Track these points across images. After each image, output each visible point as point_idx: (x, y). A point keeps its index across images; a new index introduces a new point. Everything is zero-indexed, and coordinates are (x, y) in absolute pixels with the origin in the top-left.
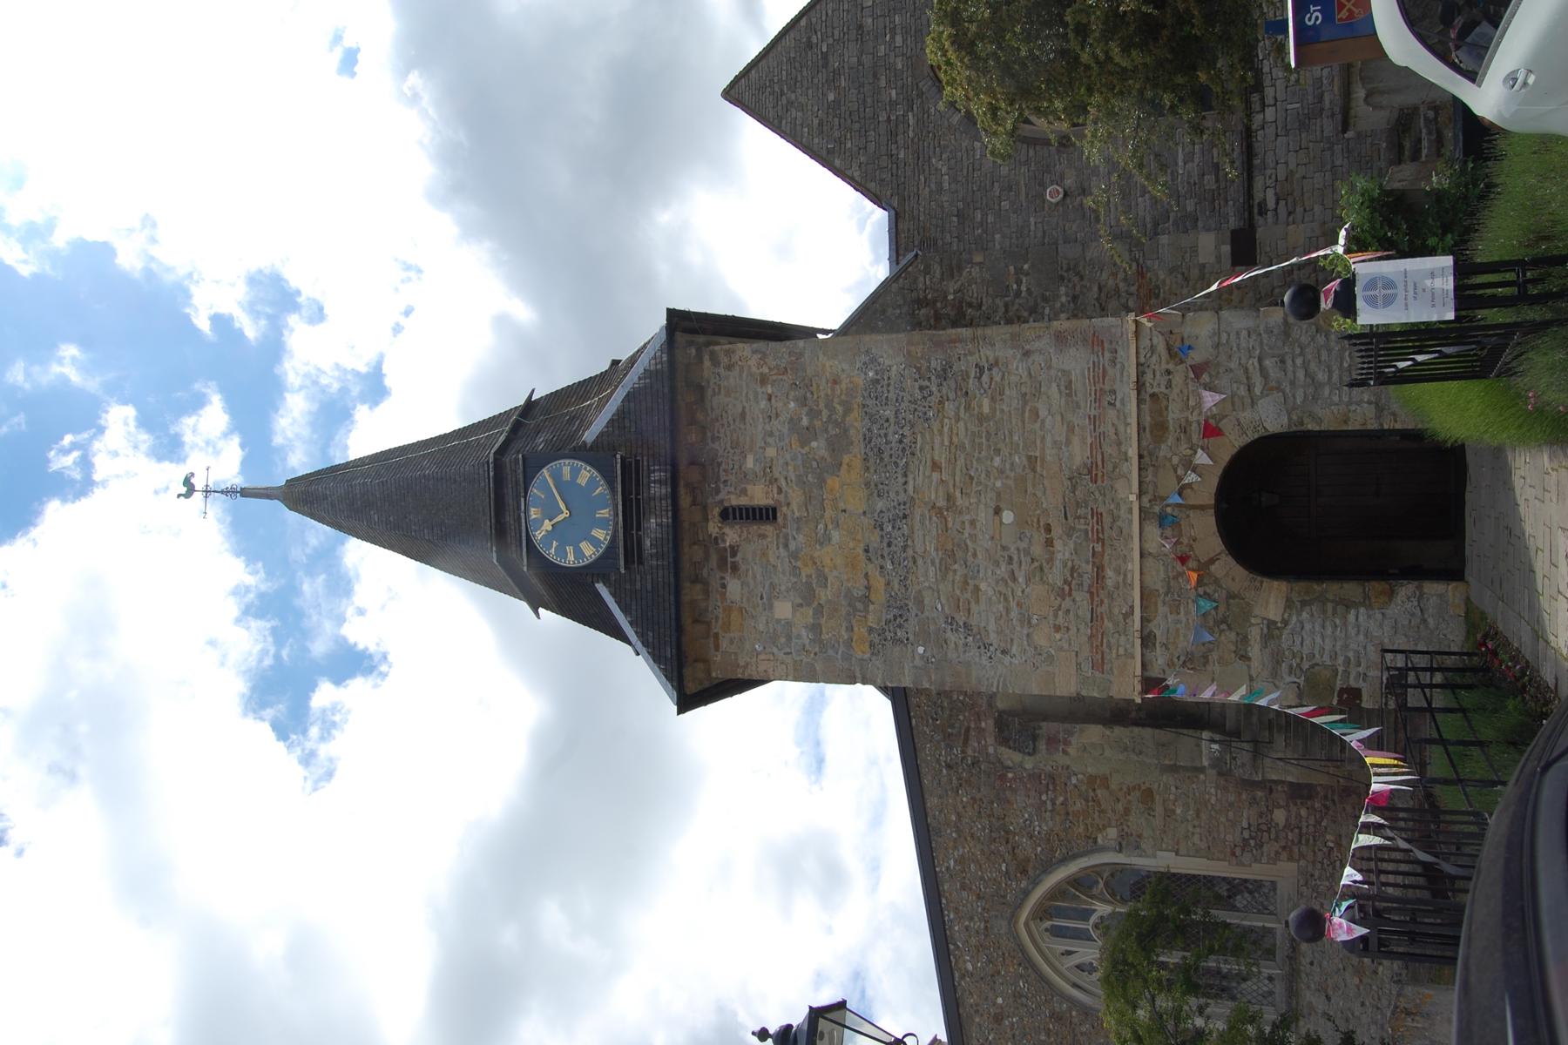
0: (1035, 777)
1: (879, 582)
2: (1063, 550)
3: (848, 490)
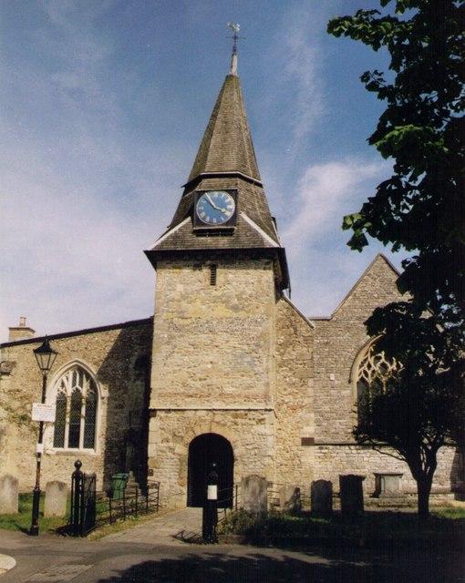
0: (127, 368)
2: (198, 384)
3: (221, 311)
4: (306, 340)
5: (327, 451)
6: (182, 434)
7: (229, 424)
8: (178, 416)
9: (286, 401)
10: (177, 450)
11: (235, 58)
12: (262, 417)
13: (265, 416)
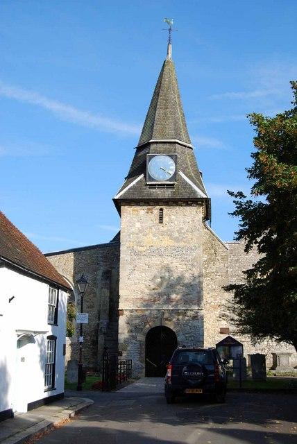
3: (167, 242)
4: (223, 258)
10: (138, 338)
11: (171, 46)
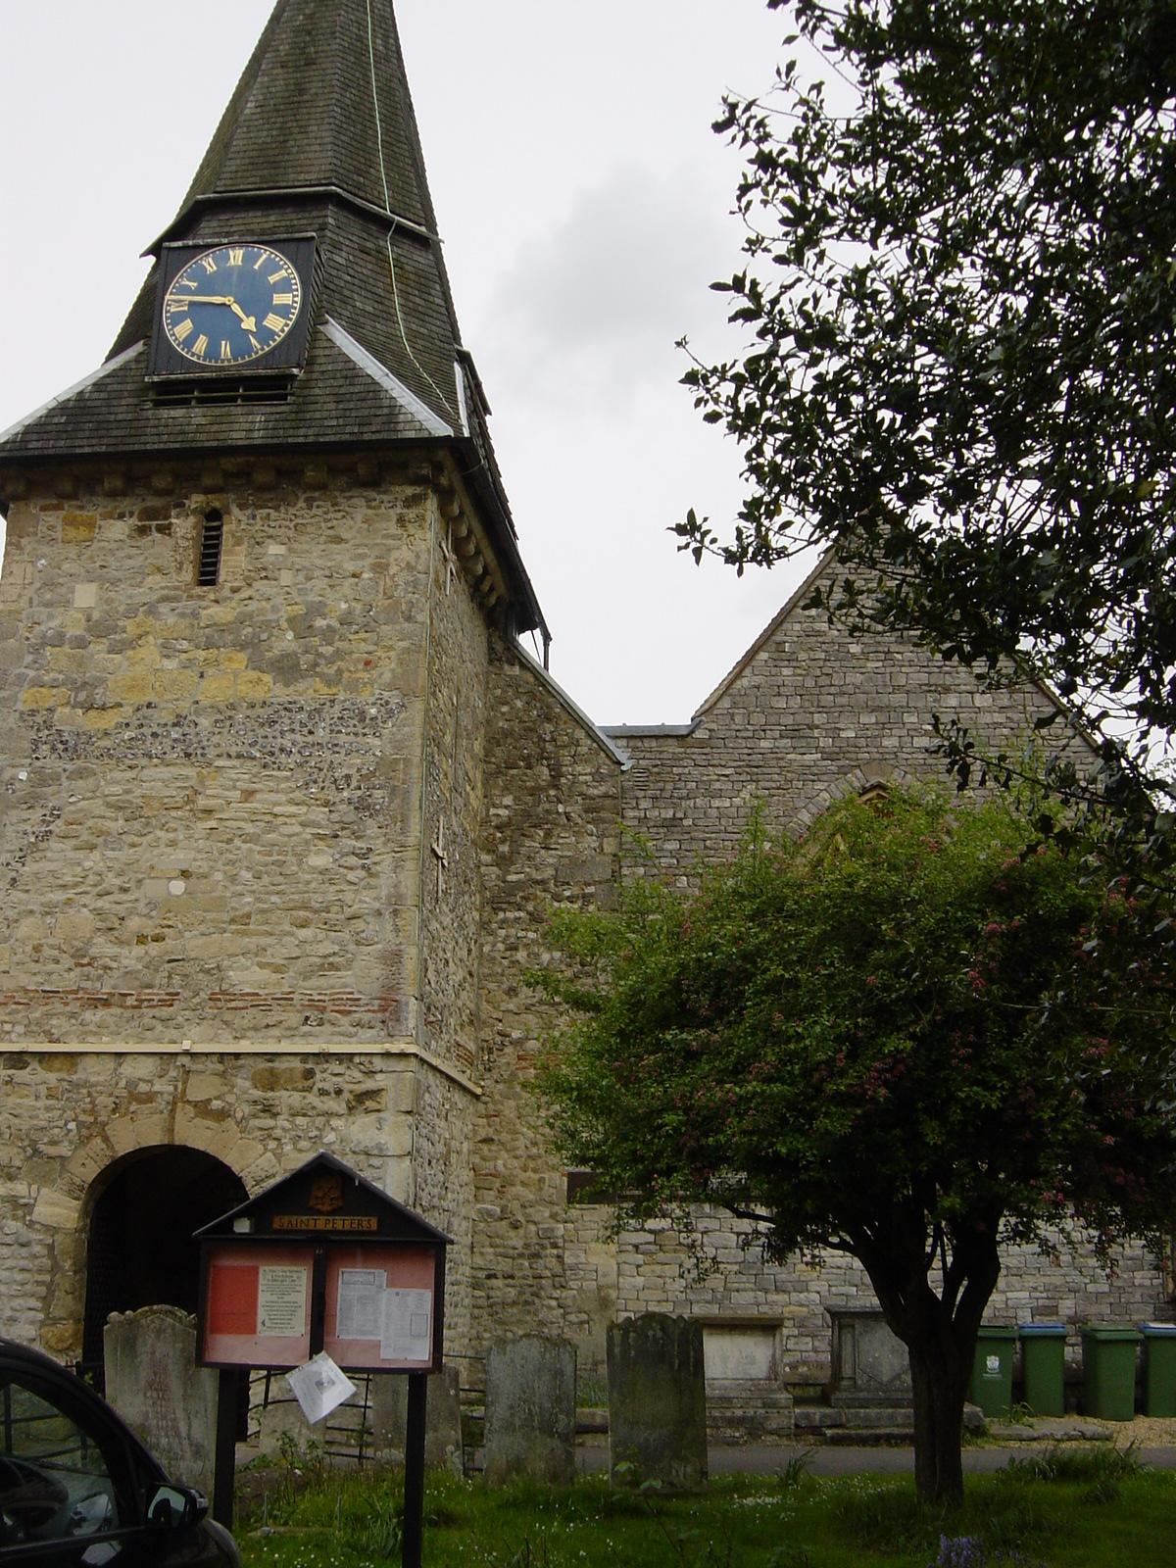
1: (110, 720)
2: (132, 957)
3: (233, 679)
4: (592, 808)
5: (665, 1223)
6: (64, 1150)
7: (242, 1110)
8: (52, 1077)
9: (516, 1035)
10: (42, 1212)
12: (370, 1084)
13: (380, 1081)
